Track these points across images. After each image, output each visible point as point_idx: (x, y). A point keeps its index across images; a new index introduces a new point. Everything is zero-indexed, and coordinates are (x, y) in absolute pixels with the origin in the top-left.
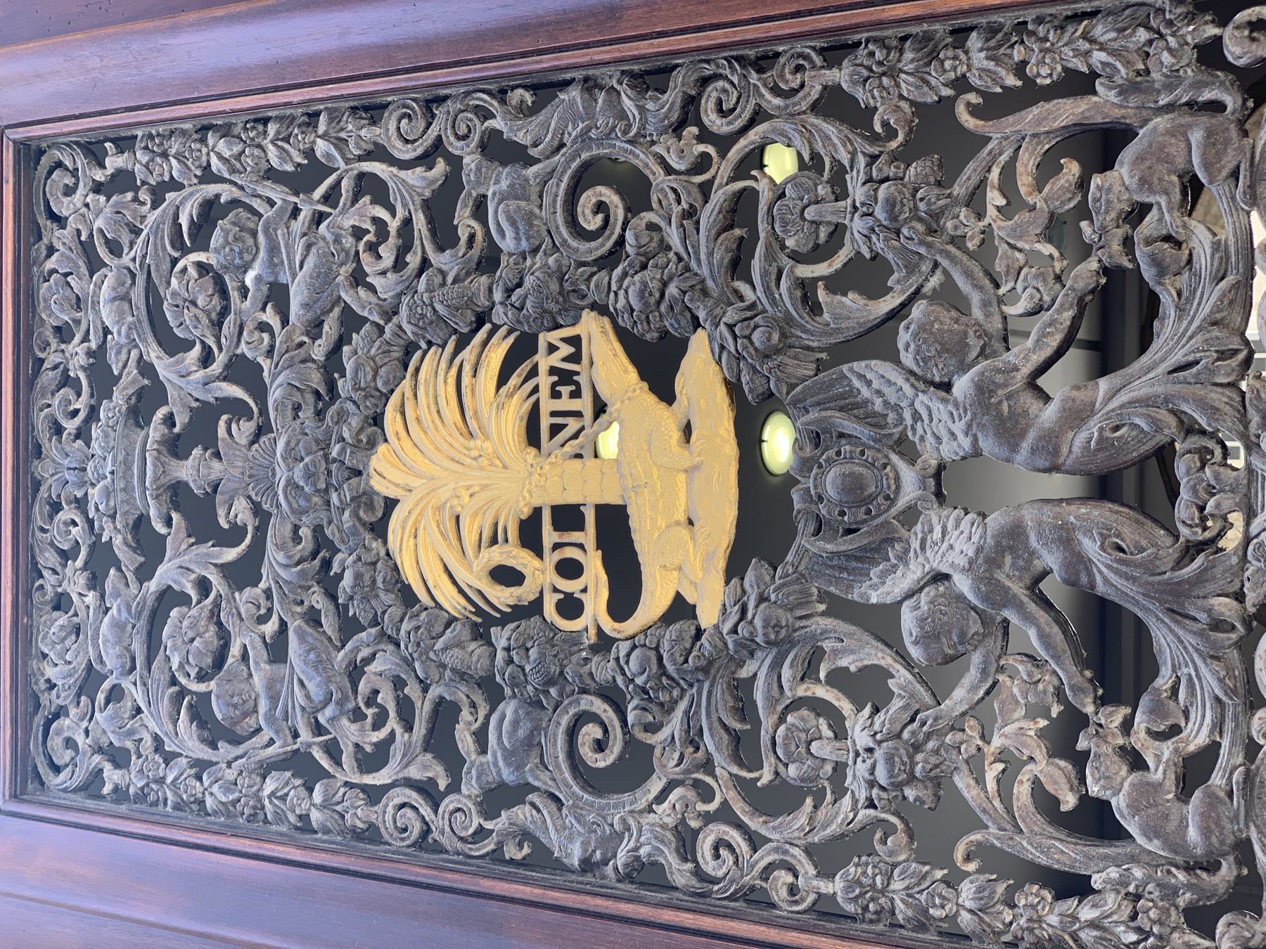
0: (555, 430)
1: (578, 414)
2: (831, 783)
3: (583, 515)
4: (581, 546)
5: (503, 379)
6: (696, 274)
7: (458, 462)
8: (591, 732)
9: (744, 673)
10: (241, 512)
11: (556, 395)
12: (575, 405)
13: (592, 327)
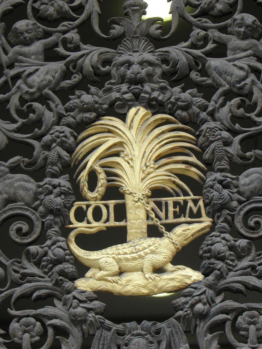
0: (159, 204)
1: (167, 217)
2: (11, 342)
3: (121, 221)
4: (107, 220)
5: (182, 177)
6: (227, 275)
7: (144, 155)
8: (25, 228)
9: (56, 301)
10: (117, 30)
11: (176, 204)
12: (171, 215)
13: (206, 222)
